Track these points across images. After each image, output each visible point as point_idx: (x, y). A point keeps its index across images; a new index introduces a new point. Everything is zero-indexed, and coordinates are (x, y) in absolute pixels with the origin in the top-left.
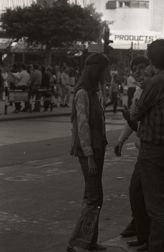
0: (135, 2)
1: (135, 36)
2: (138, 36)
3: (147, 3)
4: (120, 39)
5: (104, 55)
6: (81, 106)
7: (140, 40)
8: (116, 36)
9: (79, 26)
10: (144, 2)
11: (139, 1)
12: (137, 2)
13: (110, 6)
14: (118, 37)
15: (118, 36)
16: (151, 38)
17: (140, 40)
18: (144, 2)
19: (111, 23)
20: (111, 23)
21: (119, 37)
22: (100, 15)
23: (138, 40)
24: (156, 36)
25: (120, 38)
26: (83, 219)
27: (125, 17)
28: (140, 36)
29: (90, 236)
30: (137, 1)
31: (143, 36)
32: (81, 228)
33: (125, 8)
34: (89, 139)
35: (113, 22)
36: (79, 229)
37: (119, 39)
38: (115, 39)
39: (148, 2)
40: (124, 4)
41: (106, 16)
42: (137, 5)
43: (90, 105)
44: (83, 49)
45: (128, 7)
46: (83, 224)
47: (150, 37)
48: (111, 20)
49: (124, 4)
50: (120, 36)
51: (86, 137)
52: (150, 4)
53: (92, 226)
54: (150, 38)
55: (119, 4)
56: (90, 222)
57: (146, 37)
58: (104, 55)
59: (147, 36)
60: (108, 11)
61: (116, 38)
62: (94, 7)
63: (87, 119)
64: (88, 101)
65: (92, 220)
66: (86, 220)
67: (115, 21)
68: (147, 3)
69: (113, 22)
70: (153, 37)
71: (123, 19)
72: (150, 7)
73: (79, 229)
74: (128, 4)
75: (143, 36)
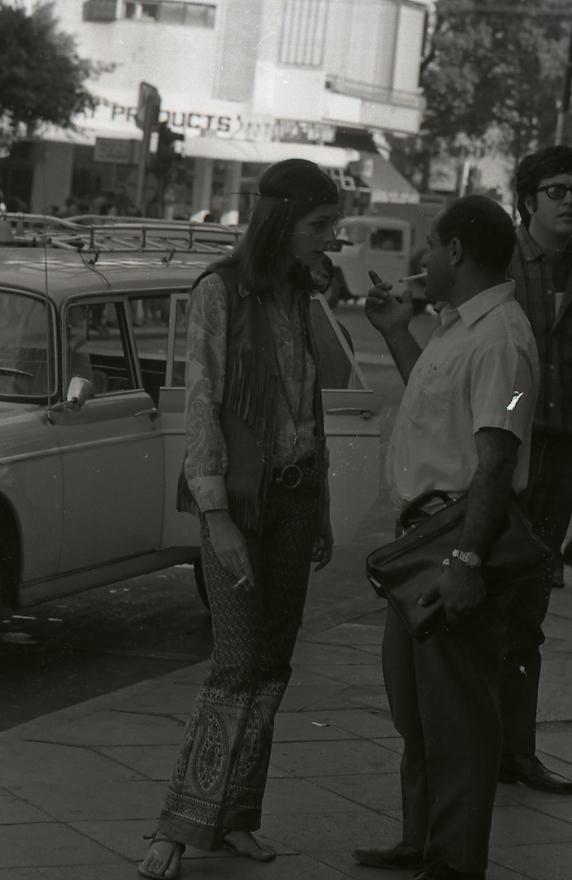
0: (174, 6)
1: (174, 114)
2: (184, 115)
3: (211, 11)
4: (128, 119)
5: (343, 179)
6: (196, 333)
7: (190, 126)
8: (115, 107)
9: (21, 72)
10: (202, 9)
11: (186, 3)
12: (181, 6)
13: (98, 11)
14: (123, 112)
15: (123, 108)
16: (225, 121)
17: (190, 126)
18: (202, 9)
19: (107, 70)
20: (110, 68)
21: (126, 111)
22: (68, 42)
23: (182, 125)
24: (239, 118)
25: (129, 115)
26: (191, 738)
27: (141, 49)
28: (191, 115)
29: (210, 802)
30: (180, 2)
31: (198, 116)
32: (185, 772)
33: (140, 21)
34: (205, 452)
35: (114, 66)
36: (179, 777)
37: (124, 117)
38: (113, 118)
39: (213, 7)
40: (139, 10)
41: (87, 42)
42: (181, 16)
43: (229, 330)
44: (10, 142)
45: (151, 19)
46: (192, 756)
47: (220, 119)
48: (108, 61)
49: (139, 10)
50: (130, 109)
51: (196, 445)
52: (219, 15)
53: (219, 763)
54: (220, 123)
55: (125, 7)
56: (213, 748)
57: (210, 118)
58: (343, 179)
59: (210, 113)
60: (89, 26)
61: (114, 113)
62: (56, 12)
63: (206, 379)
64: (222, 316)
65: (219, 740)
66: (202, 740)
67: (122, 64)
68: (211, 11)
69: (114, 66)
70: (229, 119)
71: (134, 55)
72: (218, 26)
73: (179, 777)
74: (152, 11)
75: (198, 116)
